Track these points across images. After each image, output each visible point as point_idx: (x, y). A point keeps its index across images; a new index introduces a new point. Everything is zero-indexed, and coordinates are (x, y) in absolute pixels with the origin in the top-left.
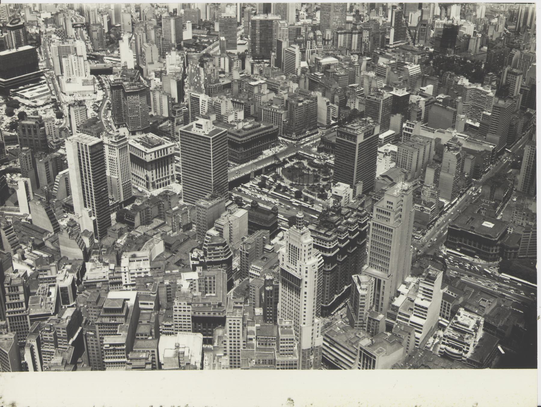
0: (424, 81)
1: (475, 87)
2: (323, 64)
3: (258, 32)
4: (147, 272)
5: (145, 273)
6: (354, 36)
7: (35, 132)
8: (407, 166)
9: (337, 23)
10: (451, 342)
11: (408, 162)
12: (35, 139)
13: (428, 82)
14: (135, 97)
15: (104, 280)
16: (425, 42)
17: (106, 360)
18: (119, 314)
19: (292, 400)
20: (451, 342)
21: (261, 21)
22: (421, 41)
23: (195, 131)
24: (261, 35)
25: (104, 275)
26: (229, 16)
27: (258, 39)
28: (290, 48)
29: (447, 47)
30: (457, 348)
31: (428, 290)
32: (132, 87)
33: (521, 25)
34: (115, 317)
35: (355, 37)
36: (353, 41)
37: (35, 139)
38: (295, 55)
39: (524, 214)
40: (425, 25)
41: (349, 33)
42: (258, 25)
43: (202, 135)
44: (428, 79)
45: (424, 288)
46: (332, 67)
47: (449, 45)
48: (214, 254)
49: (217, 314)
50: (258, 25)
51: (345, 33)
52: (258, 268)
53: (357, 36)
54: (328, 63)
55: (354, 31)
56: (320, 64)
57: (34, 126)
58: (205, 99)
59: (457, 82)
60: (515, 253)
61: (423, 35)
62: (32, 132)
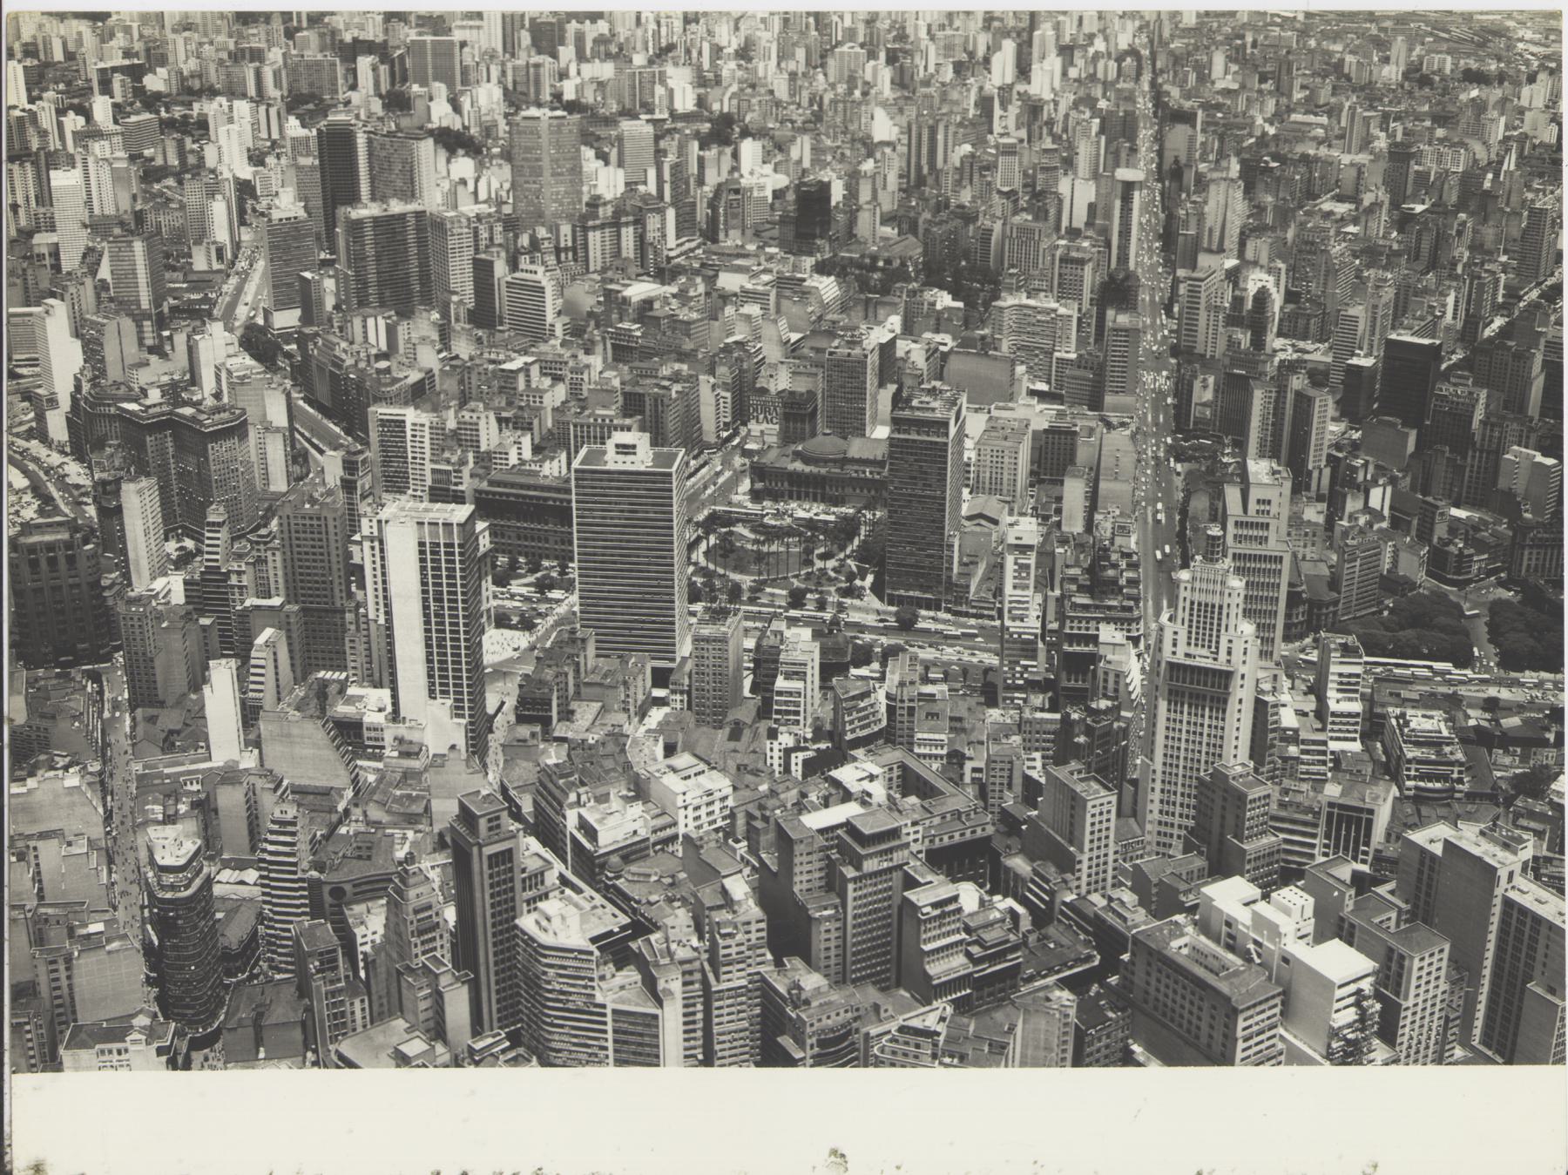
0: (871, 310)
1: (1016, 302)
2: (634, 300)
3: (370, 251)
4: (726, 798)
5: (724, 799)
6: (624, 230)
7: (71, 560)
8: (1005, 487)
9: (561, 204)
10: (1424, 768)
11: (1006, 477)
12: (71, 581)
13: (881, 312)
14: (229, 444)
15: (637, 839)
16: (743, 233)
17: (927, 947)
18: (896, 843)
19: (843, 1156)
20: (1424, 768)
21: (375, 219)
22: (731, 232)
23: (613, 461)
24: (378, 258)
25: (635, 826)
26: (292, 215)
27: (372, 268)
28: (517, 275)
29: (814, 237)
30: (1438, 778)
31: (1350, 675)
32: (217, 417)
33: (925, 170)
34: (891, 850)
35: (628, 235)
36: (624, 244)
37: (71, 581)
38: (542, 290)
39: (1306, 534)
40: (737, 191)
41: (611, 225)
42: (369, 233)
43: (642, 468)
44: (878, 303)
45: (1341, 675)
46: (657, 305)
47: (818, 231)
48: (860, 719)
49: (979, 830)
50: (369, 233)
51: (602, 227)
52: (937, 736)
53: (631, 229)
54: (643, 297)
55: (624, 219)
56: (626, 301)
57: (68, 545)
58: (419, 421)
59: (933, 304)
60: (1335, 613)
61: (735, 216)
62: (44, 565)
